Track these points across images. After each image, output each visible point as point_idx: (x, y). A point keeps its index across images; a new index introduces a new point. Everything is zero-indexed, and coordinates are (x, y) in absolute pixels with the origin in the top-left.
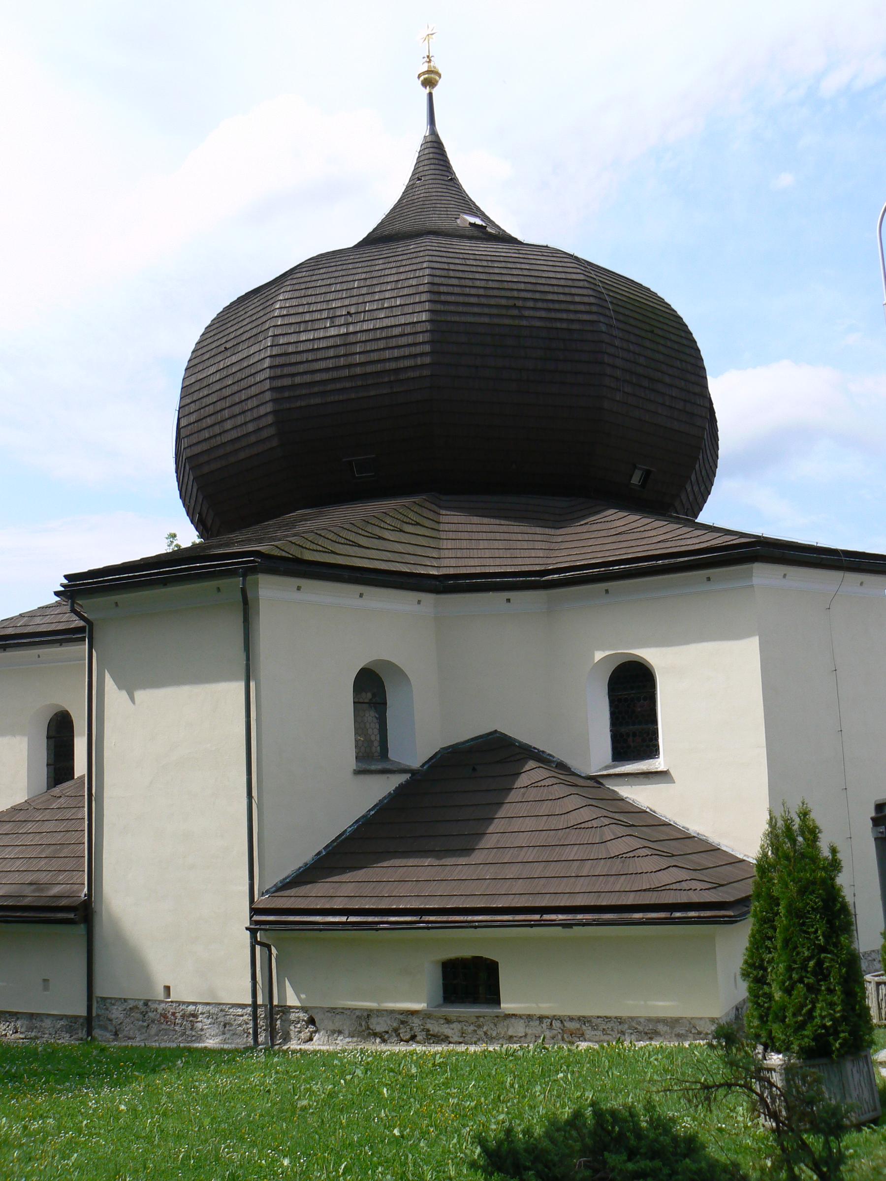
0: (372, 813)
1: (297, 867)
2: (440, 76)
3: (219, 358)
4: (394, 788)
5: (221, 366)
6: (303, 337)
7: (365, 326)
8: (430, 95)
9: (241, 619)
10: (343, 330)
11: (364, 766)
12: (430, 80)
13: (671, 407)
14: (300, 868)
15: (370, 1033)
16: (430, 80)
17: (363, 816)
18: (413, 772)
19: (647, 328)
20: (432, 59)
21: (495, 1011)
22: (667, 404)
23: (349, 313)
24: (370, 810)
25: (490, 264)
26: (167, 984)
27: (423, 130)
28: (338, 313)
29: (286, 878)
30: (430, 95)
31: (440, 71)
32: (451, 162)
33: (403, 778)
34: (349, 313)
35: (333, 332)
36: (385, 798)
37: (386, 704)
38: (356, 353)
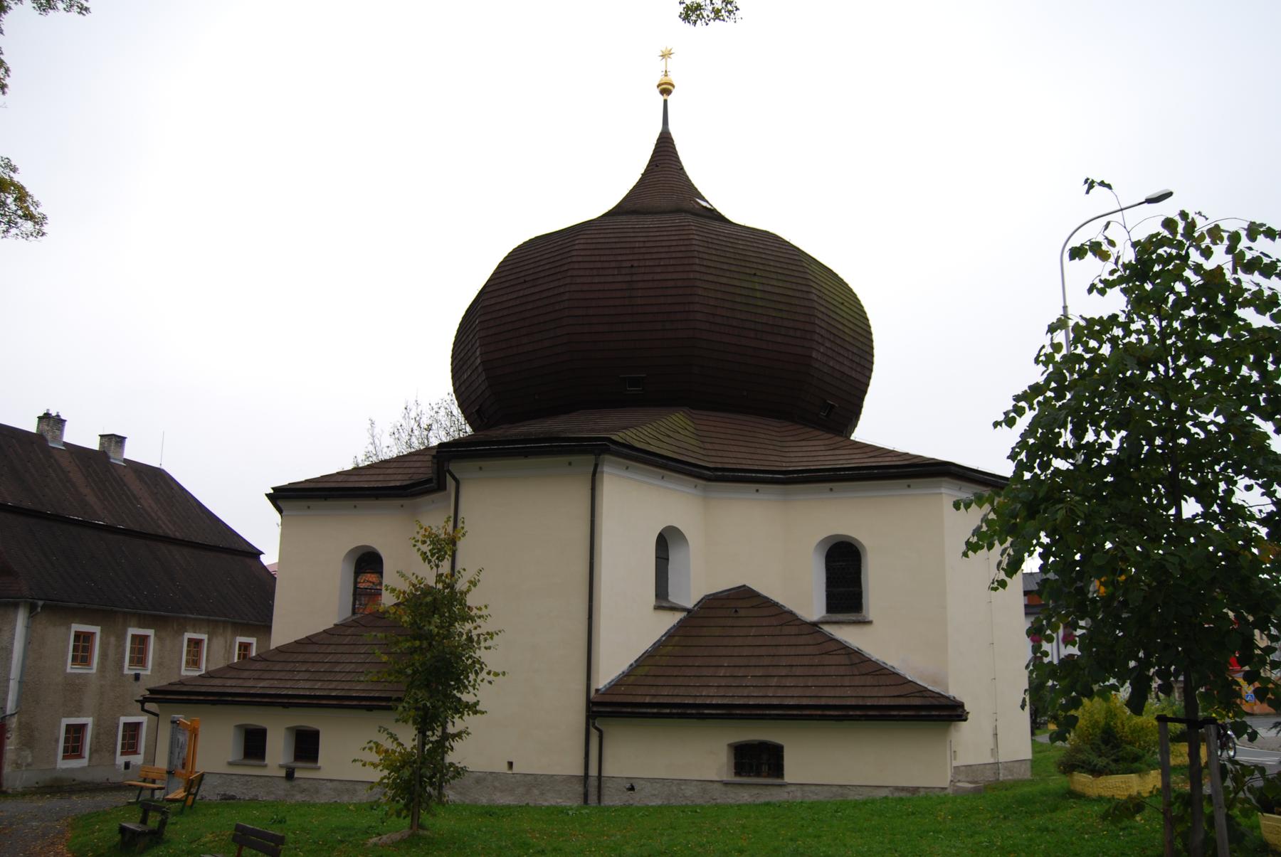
0: (664, 638)
1: (618, 674)
2: (673, 86)
3: (519, 287)
4: (676, 622)
5: (521, 293)
6: (596, 280)
7: (646, 277)
8: (665, 102)
9: (590, 487)
10: (628, 278)
11: (659, 604)
12: (666, 90)
13: (851, 360)
14: (620, 675)
15: (1160, 688)
16: (666, 90)
17: (658, 641)
18: (689, 611)
19: (841, 301)
20: (668, 73)
21: (778, 781)
22: (850, 357)
23: (632, 266)
24: (662, 636)
25: (736, 241)
26: (510, 761)
27: (1146, 204)
28: (625, 264)
29: (611, 682)
30: (665, 102)
31: (675, 84)
32: (679, 154)
33: (679, 616)
34: (632, 266)
35: (620, 278)
36: (671, 628)
37: (668, 559)
38: (638, 297)
